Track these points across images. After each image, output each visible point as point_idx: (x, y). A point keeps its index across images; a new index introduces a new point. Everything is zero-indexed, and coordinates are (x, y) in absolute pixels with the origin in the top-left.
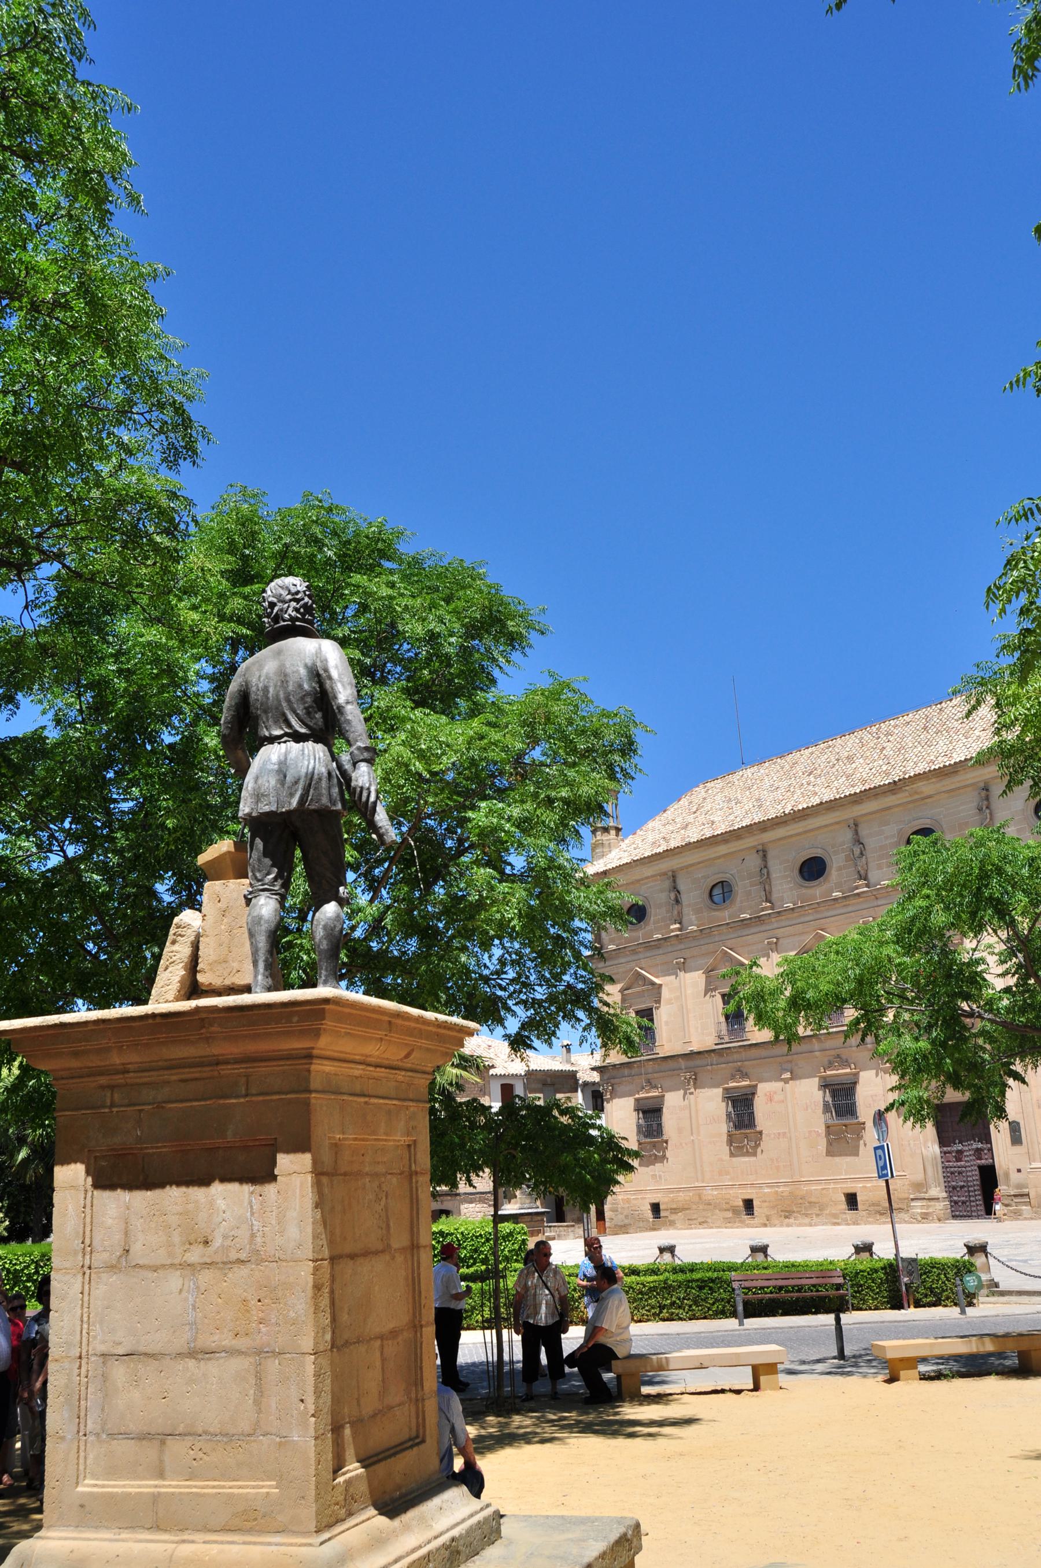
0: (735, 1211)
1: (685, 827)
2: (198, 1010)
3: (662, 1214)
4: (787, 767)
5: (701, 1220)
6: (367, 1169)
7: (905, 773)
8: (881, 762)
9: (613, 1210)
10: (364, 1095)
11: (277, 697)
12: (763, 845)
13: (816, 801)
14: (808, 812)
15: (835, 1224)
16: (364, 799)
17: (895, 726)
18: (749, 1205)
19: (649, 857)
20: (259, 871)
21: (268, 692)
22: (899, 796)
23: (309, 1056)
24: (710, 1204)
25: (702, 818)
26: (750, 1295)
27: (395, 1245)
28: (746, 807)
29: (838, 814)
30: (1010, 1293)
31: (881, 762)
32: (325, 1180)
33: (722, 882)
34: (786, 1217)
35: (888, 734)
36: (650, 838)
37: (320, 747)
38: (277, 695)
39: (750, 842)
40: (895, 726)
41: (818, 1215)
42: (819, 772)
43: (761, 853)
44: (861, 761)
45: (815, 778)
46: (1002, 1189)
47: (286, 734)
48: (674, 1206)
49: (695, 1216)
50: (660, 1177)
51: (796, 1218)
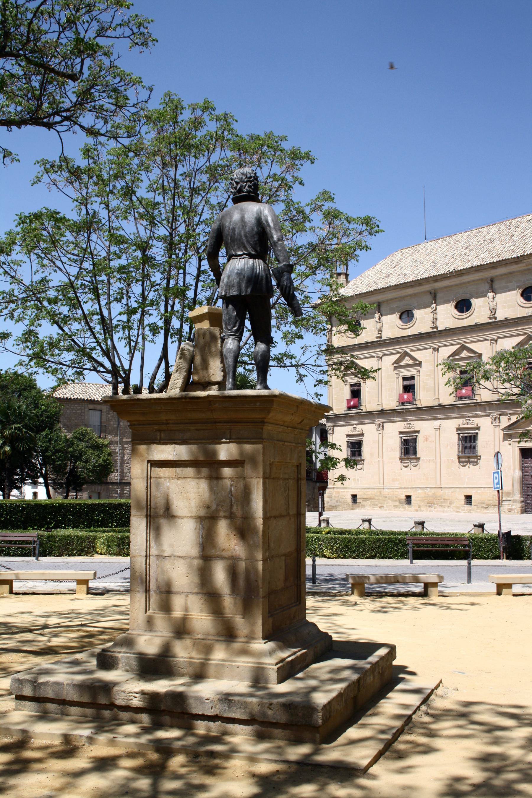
0: (400, 502)
2: (208, 396)
3: (358, 501)
4: (453, 243)
5: (379, 505)
6: (281, 476)
7: (524, 252)
8: (510, 244)
9: (330, 497)
10: (281, 441)
11: (240, 234)
12: (435, 290)
13: (469, 265)
14: (464, 272)
15: (457, 512)
16: (287, 292)
17: (521, 222)
18: (409, 498)
19: (365, 293)
20: (229, 325)
21: (235, 231)
22: (520, 265)
23: (263, 422)
24: (386, 497)
25: (398, 271)
26: (416, 548)
27: (291, 513)
28: (426, 266)
31: (510, 244)
32: (267, 481)
33: (408, 311)
34: (430, 506)
35: (516, 227)
36: (366, 282)
37: (261, 261)
38: (240, 233)
39: (427, 287)
40: (521, 222)
42: (472, 247)
43: (433, 295)
44: (499, 242)
45: (470, 251)
47: (244, 254)
48: (365, 497)
49: (377, 503)
50: (358, 480)
51: (435, 508)
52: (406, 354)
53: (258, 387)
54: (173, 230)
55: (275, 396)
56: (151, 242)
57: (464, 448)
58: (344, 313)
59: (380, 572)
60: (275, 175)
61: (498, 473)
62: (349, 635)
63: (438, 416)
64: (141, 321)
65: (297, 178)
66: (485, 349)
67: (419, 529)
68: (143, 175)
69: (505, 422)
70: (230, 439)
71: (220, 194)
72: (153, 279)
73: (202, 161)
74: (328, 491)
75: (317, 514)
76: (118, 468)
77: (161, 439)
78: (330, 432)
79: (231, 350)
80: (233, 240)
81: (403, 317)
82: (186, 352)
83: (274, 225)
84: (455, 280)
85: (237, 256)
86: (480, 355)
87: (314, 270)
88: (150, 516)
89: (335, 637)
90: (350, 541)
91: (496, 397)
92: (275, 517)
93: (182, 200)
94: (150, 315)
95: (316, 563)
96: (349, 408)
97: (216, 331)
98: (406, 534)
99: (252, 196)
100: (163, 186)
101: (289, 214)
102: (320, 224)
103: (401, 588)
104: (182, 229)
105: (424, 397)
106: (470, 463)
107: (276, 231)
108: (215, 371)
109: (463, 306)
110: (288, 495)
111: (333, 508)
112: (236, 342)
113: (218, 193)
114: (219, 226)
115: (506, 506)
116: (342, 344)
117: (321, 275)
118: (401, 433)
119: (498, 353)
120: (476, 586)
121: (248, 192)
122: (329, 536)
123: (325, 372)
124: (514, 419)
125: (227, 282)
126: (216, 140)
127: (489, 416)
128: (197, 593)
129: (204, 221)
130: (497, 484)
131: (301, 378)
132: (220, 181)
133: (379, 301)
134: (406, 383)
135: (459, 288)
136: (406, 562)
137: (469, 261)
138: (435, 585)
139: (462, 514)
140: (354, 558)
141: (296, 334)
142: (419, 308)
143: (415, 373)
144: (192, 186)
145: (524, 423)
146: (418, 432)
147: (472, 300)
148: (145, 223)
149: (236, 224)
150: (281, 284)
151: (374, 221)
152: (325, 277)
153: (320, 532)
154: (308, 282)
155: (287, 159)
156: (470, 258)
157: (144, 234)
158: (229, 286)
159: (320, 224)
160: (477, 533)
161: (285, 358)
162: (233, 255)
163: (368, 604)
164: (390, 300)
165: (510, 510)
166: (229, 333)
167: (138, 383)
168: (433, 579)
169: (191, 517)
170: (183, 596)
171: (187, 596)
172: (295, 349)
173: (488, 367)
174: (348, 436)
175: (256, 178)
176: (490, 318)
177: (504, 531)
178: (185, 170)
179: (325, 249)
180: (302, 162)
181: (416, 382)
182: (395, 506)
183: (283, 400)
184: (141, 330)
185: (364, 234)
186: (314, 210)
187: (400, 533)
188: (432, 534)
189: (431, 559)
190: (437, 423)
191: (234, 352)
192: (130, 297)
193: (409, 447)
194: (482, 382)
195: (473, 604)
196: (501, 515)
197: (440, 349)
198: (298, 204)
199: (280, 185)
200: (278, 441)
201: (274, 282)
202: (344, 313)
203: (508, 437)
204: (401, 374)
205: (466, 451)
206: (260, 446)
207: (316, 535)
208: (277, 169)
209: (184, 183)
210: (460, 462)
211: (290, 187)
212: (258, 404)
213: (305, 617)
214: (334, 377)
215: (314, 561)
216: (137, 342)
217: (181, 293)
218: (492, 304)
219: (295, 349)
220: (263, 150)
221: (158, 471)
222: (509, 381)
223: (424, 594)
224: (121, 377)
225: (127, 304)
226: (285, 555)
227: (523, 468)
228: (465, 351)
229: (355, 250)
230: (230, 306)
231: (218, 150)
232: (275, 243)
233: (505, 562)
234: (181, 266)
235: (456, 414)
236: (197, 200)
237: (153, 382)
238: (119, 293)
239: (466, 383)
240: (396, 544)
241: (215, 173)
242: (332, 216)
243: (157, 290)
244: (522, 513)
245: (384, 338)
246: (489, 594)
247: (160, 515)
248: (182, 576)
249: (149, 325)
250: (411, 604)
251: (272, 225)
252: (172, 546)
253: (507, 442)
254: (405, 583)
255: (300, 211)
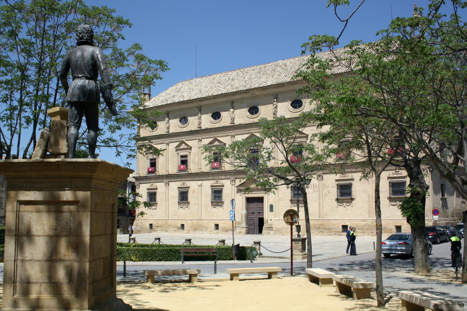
0: (178, 228)
1: (174, 97)
2: (57, 162)
4: (211, 80)
7: (251, 87)
9: (137, 225)
10: (103, 190)
13: (220, 93)
15: (210, 234)
17: (249, 70)
18: (183, 226)
23: (91, 178)
24: (169, 225)
25: (180, 94)
26: (186, 254)
27: (108, 233)
29: (227, 98)
30: (265, 257)
32: (93, 213)
35: (247, 72)
36: (161, 99)
37: (93, 81)
39: (196, 104)
40: (249, 70)
41: (205, 231)
46: (265, 226)
52: (183, 142)
53: (89, 157)
54: (42, 60)
55: (99, 163)
56: (27, 67)
57: (215, 197)
58: (148, 117)
59: (164, 269)
60: (107, 32)
61: (233, 211)
62: (144, 306)
63: (201, 179)
64: (19, 115)
65: (120, 35)
66: (227, 140)
67: (188, 243)
68: (24, 25)
69: (238, 182)
70: (70, 188)
71: (72, 41)
72: (28, 90)
73: (62, 20)
74: (135, 222)
75: (128, 235)
76: (3, 207)
77: (26, 187)
78: (138, 187)
79: (72, 134)
80: (76, 68)
81: (182, 121)
82: (45, 135)
83: (102, 60)
84: (212, 101)
85: (79, 77)
86: (225, 144)
87: (128, 90)
88: (18, 235)
89: (134, 307)
90: (147, 251)
91: (233, 169)
92: (98, 235)
93: (48, 42)
94: (26, 112)
95: (126, 264)
96: (149, 172)
97: (64, 122)
98: (180, 246)
99: (90, 42)
100: (36, 32)
101: (115, 56)
102: (133, 63)
103: (177, 278)
104: (48, 60)
105: (193, 168)
106: (218, 205)
107: (103, 64)
108: (63, 147)
109: (216, 116)
110: (106, 222)
111: (139, 232)
112: (76, 130)
113: (72, 40)
114: (68, 58)
115: (238, 230)
116: (146, 135)
117: (133, 93)
118: (179, 188)
119: (234, 142)
120: (219, 276)
121: (87, 39)
122: (135, 248)
123: (133, 150)
124: (243, 181)
125: (72, 93)
126: (72, 8)
127: (229, 179)
128: (47, 283)
129: (62, 56)
130: (232, 217)
131: (118, 154)
132: (73, 32)
133: (168, 111)
134: (182, 159)
135: (213, 106)
136: (180, 263)
137: (220, 90)
138: (196, 275)
139: (213, 235)
140: (149, 261)
141: (117, 127)
142: (191, 116)
143: (188, 153)
144: (55, 34)
145: (248, 183)
146: (189, 187)
147: (221, 113)
148: (24, 54)
149: (79, 58)
150: (105, 96)
151: (164, 63)
152: (135, 94)
153: (130, 246)
154: (124, 97)
155: (114, 23)
156: (221, 89)
157: (22, 61)
158: (73, 95)
159: (133, 63)
160: (220, 245)
161: (110, 141)
162: (76, 77)
163: (157, 288)
164: (175, 110)
165: (240, 233)
166: (72, 124)
167: (16, 154)
168: (195, 272)
169: (44, 236)
170: (39, 285)
171: (41, 285)
172: (116, 136)
173: (228, 150)
174: (148, 189)
175: (92, 31)
176: (231, 123)
177: (236, 244)
178: (51, 24)
179: (135, 78)
180: (123, 25)
181: (188, 159)
182: (175, 231)
183: (104, 164)
184: (18, 121)
185: (159, 70)
186: (129, 54)
187: (177, 246)
188: (195, 246)
189: (194, 261)
190: (200, 183)
191: (75, 135)
192: (12, 100)
193: (184, 196)
194: (224, 158)
195: (217, 286)
196: (234, 235)
197: (202, 140)
198: (120, 50)
199: (110, 38)
200: (101, 189)
201: (101, 95)
202: (148, 117)
203: (239, 191)
204: (180, 154)
205: (216, 199)
206: (89, 193)
207: (127, 248)
208: (108, 29)
209: (51, 32)
210: (212, 205)
211: (116, 40)
212: (88, 167)
213: (115, 296)
214: (138, 153)
215: (125, 263)
216: (15, 128)
217: (45, 98)
218: (232, 116)
219: (116, 136)
220: (101, 16)
221: (23, 207)
222: (239, 158)
223: (189, 281)
224: (5, 150)
225: (10, 104)
226: (103, 258)
227: (247, 209)
228: (216, 142)
229: (153, 79)
230: (73, 108)
231: (73, 14)
232: (102, 72)
233: (236, 262)
234: (46, 83)
235: (211, 178)
236: (58, 43)
237: (26, 154)
238: (5, 97)
239: (216, 160)
240: (174, 253)
241: (70, 27)
242: (140, 58)
243: (30, 96)
244: (246, 234)
245: (170, 132)
246: (226, 280)
247: (23, 236)
248: (36, 272)
249: (25, 117)
250: (182, 287)
251: (100, 60)
252: (32, 254)
253: (239, 194)
254: (179, 275)
255: (121, 54)
